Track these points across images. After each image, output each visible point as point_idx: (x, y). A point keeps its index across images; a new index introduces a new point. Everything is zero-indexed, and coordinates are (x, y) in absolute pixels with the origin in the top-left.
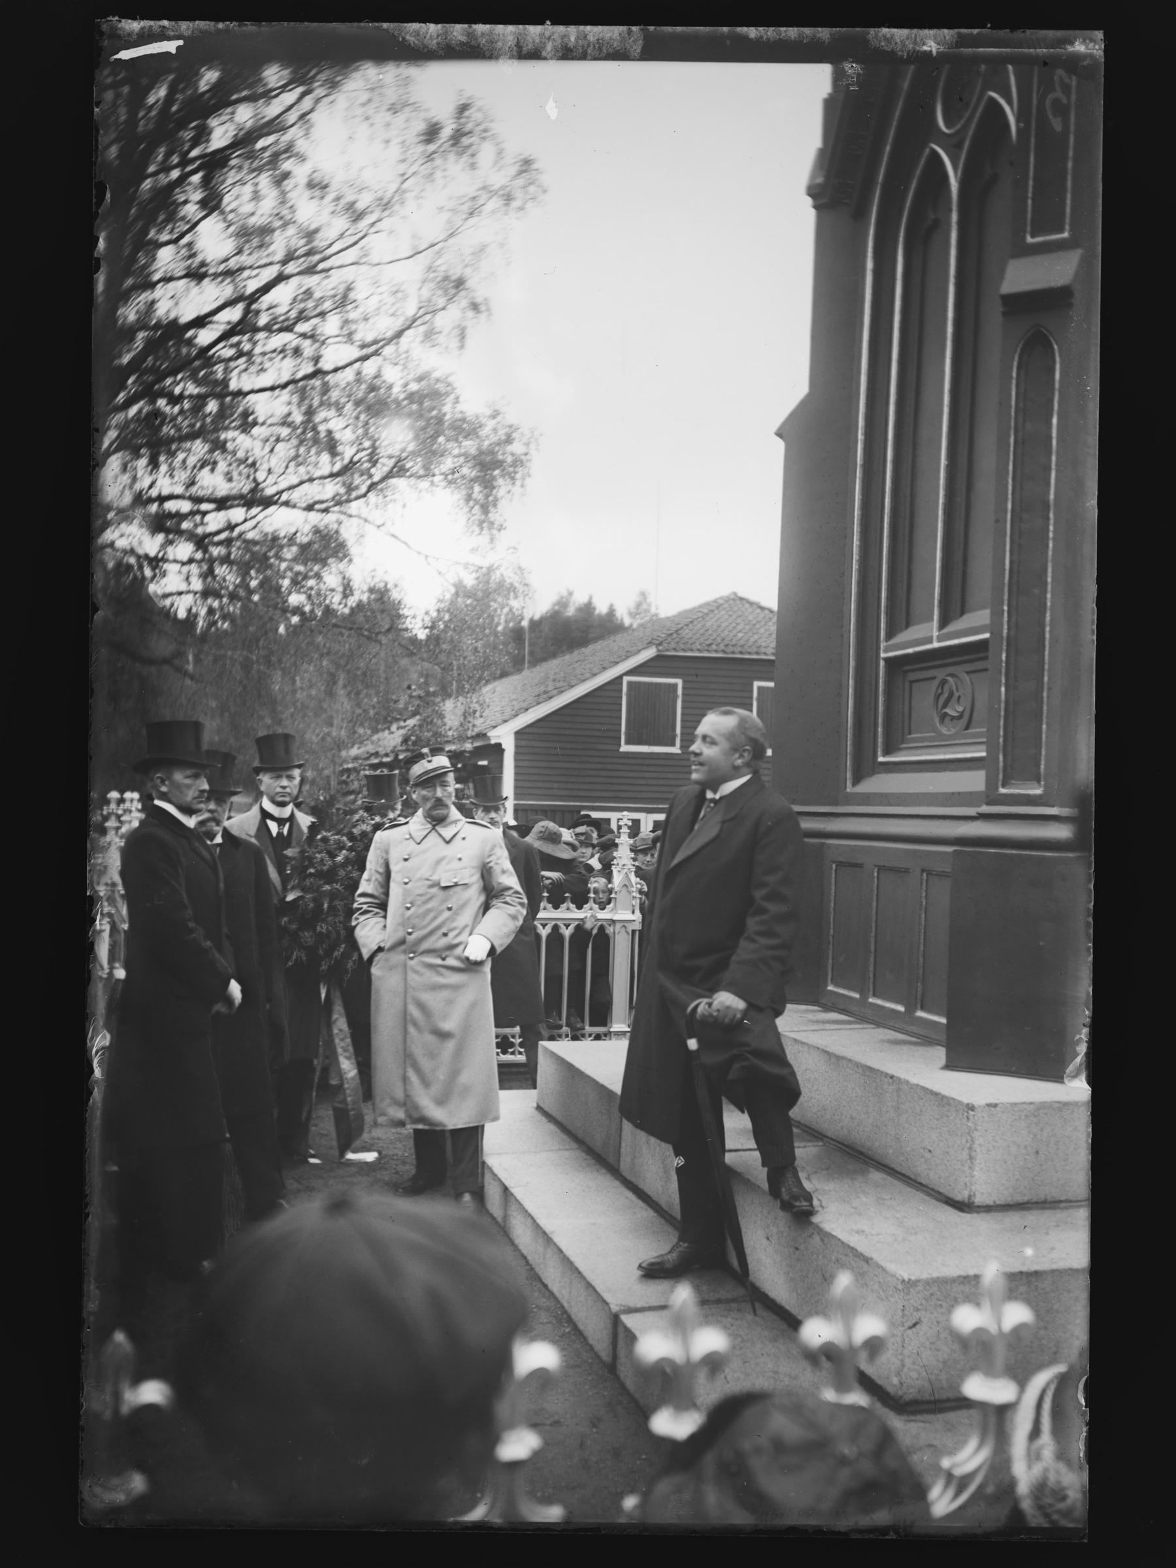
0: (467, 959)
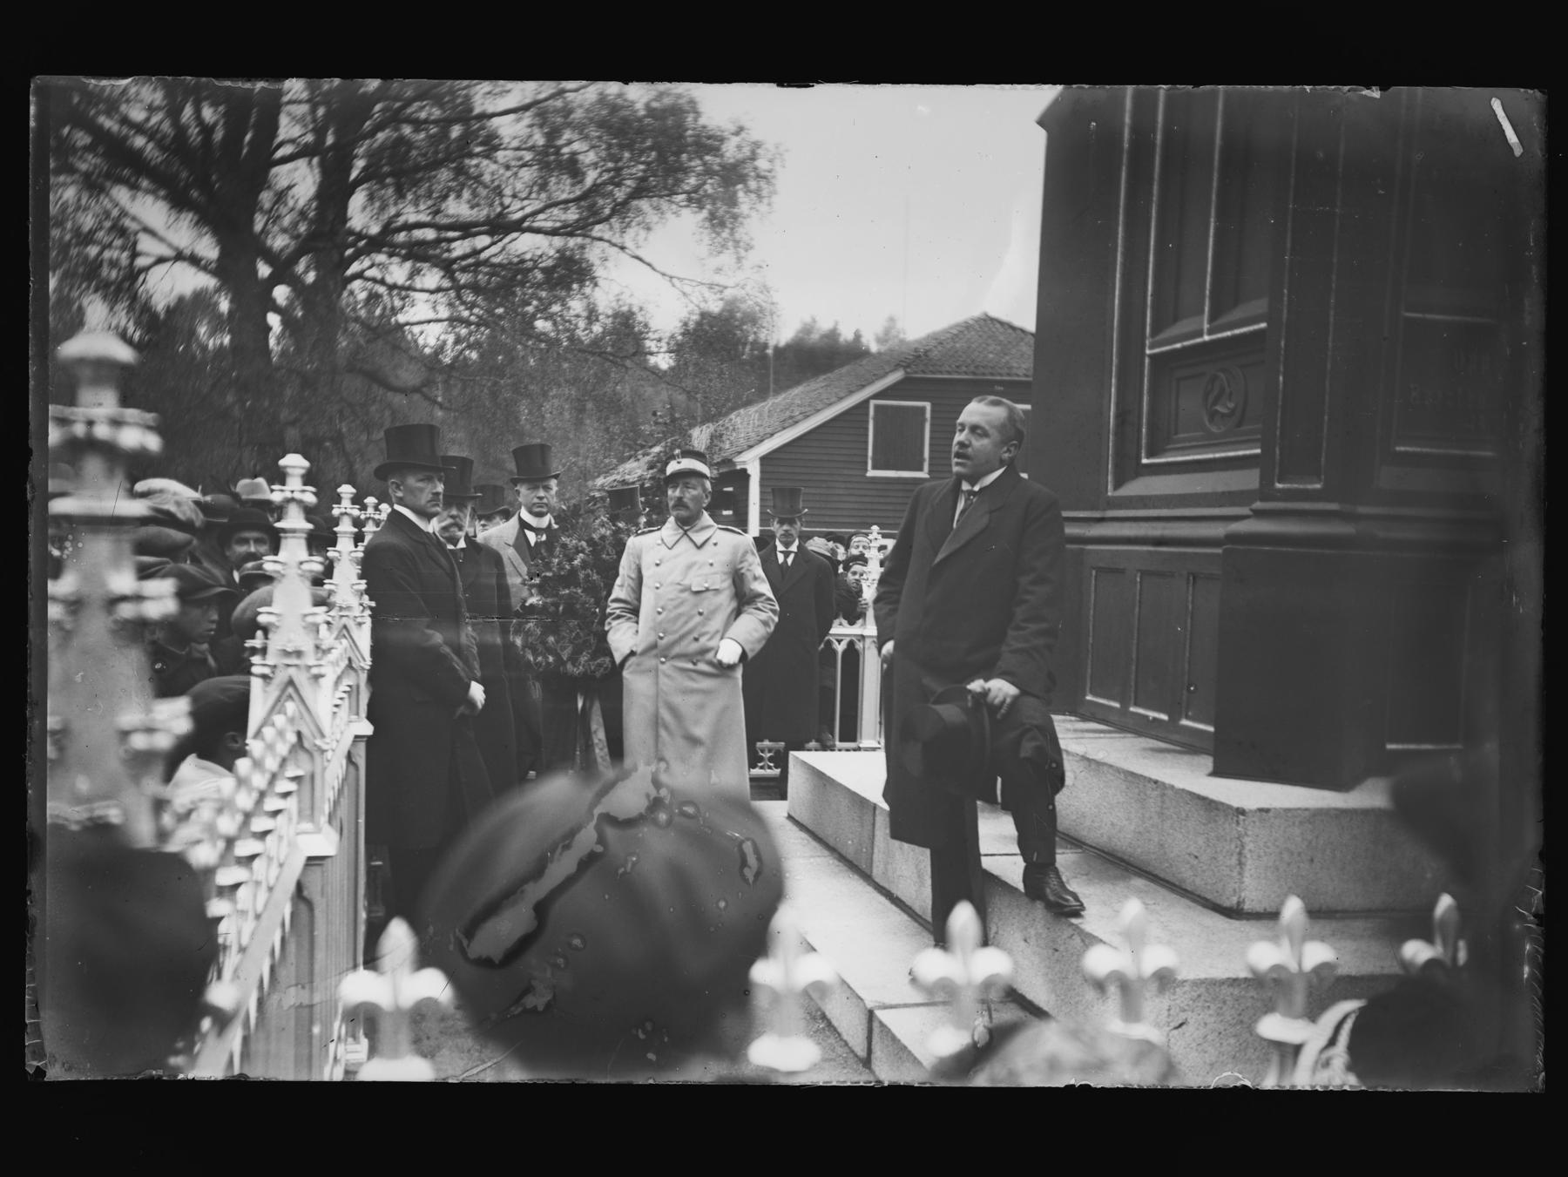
0: (720, 663)
